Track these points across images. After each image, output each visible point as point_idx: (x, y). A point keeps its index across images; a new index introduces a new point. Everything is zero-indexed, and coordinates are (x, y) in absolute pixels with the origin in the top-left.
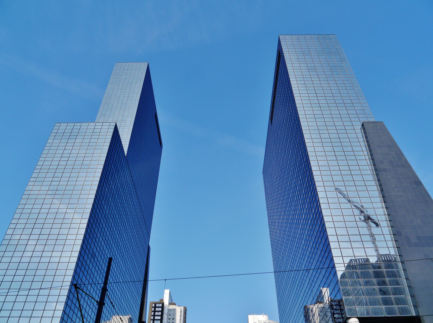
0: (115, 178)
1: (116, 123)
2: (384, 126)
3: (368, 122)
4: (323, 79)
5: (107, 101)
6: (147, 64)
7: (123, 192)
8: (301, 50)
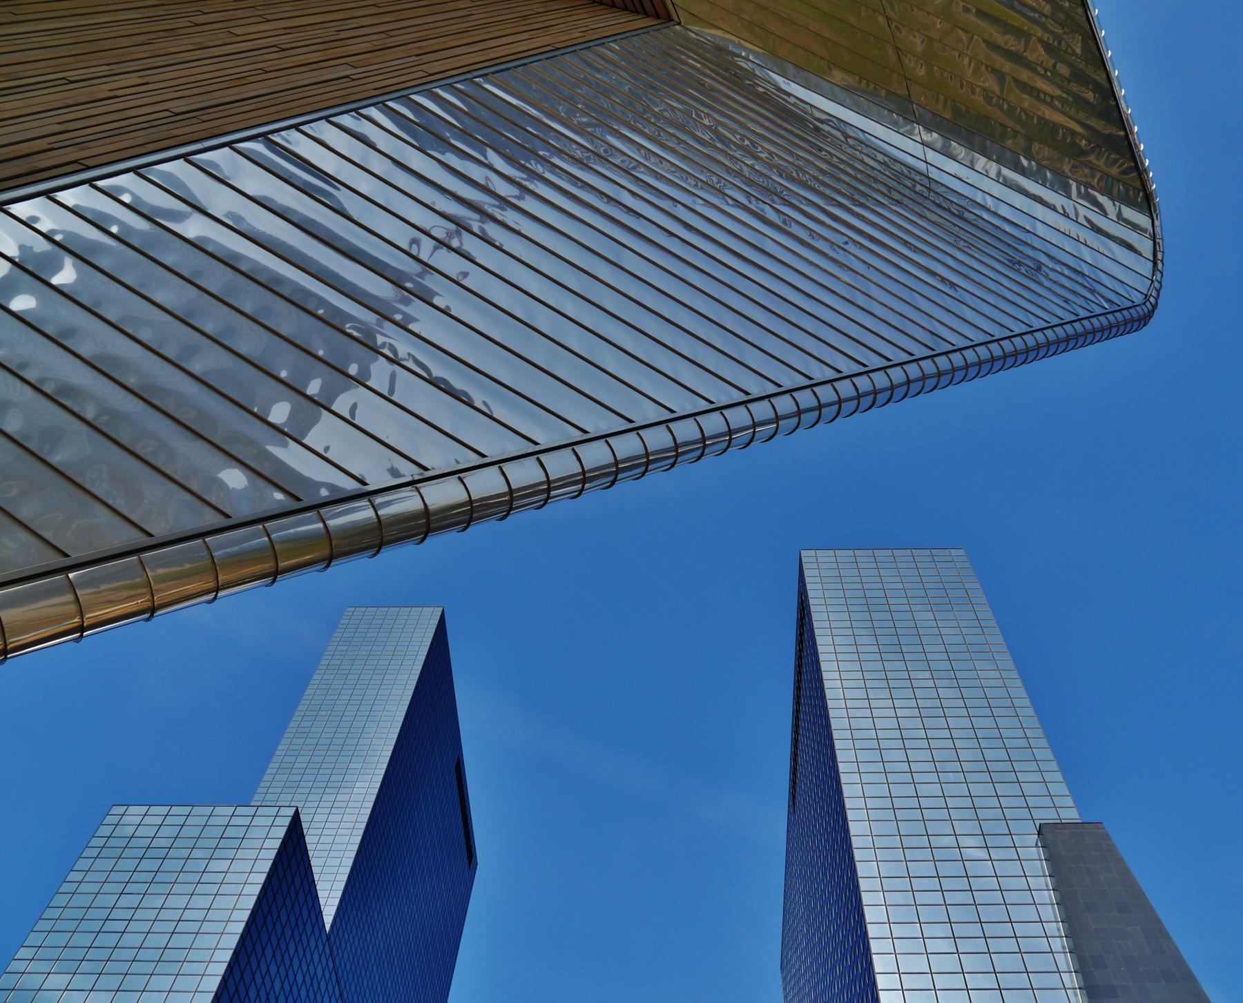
0: (287, 953)
1: (297, 810)
2: (1107, 837)
3: (1059, 821)
4: (914, 657)
5: (303, 724)
6: (438, 612)
7: (308, 986)
8: (861, 594)
